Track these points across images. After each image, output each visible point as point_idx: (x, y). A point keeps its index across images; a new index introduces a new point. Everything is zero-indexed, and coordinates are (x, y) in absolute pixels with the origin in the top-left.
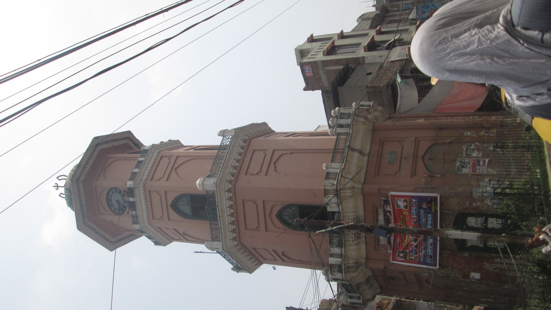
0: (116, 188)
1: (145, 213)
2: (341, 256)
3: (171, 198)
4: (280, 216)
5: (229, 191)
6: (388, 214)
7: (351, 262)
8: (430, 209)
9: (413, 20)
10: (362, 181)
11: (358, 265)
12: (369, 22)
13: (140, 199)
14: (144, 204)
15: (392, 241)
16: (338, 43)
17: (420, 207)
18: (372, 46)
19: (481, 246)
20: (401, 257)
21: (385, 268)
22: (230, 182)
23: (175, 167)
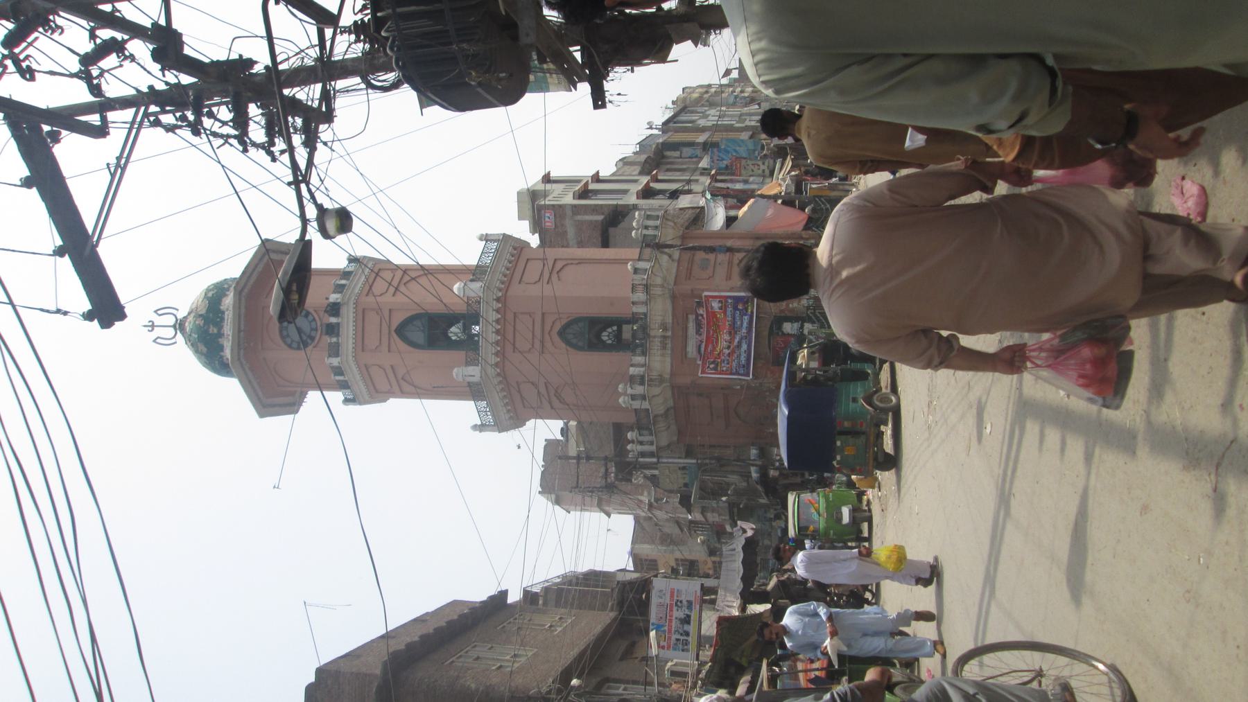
1: (351, 341)
4: (562, 333)
5: (498, 300)
7: (655, 374)
8: (746, 309)
11: (661, 380)
12: (637, 169)
13: (347, 321)
14: (351, 328)
16: (592, 186)
17: (736, 308)
18: (647, 193)
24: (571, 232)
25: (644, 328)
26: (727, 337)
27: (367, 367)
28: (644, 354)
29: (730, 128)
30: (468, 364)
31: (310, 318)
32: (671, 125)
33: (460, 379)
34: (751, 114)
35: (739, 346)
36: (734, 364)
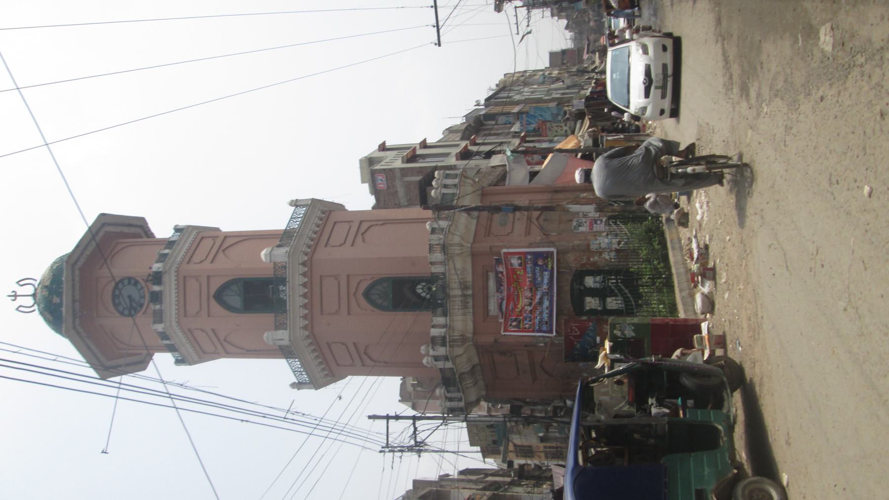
0: (130, 279)
1: (174, 307)
2: (445, 326)
3: (216, 284)
4: (367, 294)
5: (304, 264)
6: (500, 275)
8: (547, 266)
9: (516, 133)
10: (472, 241)
11: (463, 339)
12: (460, 135)
13: (170, 289)
14: (174, 295)
15: (504, 307)
16: (419, 152)
17: (535, 264)
18: (465, 155)
19: (599, 308)
20: (514, 327)
21: (496, 341)
22: (306, 254)
23: (222, 248)
24: (401, 192)
25: (444, 288)
26: (528, 294)
27: (189, 330)
28: (445, 314)
29: (539, 101)
30: (277, 328)
31: (139, 286)
32: (493, 100)
33: (271, 343)
34: (556, 89)
35: (541, 302)
36: (537, 321)
